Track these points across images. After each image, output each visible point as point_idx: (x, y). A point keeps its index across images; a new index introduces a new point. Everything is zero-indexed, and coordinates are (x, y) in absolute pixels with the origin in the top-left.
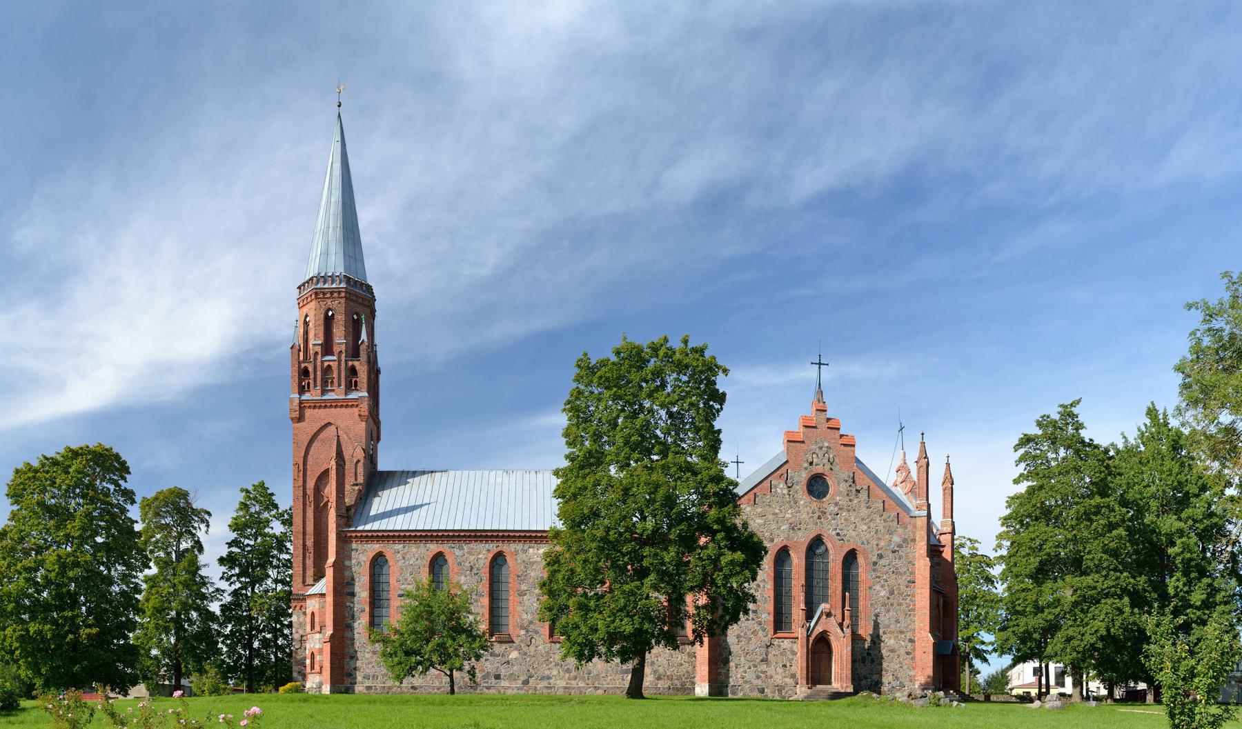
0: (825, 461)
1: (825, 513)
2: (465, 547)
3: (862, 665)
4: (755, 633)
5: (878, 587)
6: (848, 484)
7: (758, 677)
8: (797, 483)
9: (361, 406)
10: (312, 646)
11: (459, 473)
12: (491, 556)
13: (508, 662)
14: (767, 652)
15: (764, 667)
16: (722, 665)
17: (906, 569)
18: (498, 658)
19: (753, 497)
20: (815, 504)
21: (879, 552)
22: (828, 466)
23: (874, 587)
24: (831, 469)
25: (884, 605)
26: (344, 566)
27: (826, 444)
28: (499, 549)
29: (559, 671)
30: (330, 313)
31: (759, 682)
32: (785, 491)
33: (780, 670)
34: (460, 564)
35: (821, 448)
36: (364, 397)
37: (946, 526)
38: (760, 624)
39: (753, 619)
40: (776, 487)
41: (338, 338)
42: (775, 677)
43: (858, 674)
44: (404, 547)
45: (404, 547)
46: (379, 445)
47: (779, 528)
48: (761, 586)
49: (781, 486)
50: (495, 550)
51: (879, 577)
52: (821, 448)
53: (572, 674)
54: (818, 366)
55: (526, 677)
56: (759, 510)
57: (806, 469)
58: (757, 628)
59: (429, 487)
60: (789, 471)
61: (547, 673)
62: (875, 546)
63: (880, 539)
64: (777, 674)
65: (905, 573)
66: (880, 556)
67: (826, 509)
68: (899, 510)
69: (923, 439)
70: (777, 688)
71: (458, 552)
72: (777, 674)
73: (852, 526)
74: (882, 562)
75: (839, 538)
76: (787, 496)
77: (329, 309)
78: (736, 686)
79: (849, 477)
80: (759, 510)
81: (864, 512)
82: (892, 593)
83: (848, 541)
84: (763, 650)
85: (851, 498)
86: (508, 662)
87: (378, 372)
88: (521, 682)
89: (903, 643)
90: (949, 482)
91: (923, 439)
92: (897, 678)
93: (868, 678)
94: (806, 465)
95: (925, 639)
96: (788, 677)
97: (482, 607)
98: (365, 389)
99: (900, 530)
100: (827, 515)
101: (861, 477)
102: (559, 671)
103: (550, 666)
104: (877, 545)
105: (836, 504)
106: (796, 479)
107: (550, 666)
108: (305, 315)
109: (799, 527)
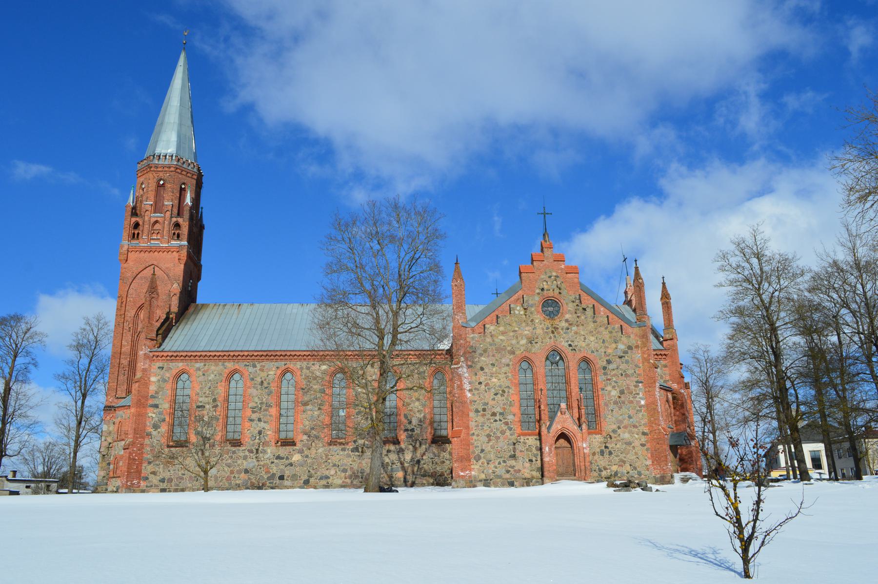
0: (555, 287)
1: (558, 328)
2: (258, 365)
3: (601, 457)
4: (503, 432)
5: (609, 388)
6: (575, 304)
7: (508, 472)
8: (532, 306)
9: (182, 252)
10: (116, 453)
11: (262, 305)
12: (279, 372)
13: (291, 465)
14: (515, 448)
15: (512, 462)
16: (475, 462)
17: (633, 371)
18: (282, 461)
19: (495, 318)
20: (548, 321)
21: (607, 358)
22: (557, 291)
23: (606, 388)
24: (560, 293)
25: (616, 403)
26: (150, 381)
27: (554, 274)
28: (286, 366)
29: (336, 472)
30: (162, 182)
31: (508, 476)
32: (522, 313)
33: (527, 465)
34: (252, 379)
35: (550, 277)
36: (184, 246)
37: (668, 333)
38: (506, 424)
39: (500, 420)
40: (514, 310)
41: (166, 201)
42: (523, 471)
43: (598, 466)
44: (205, 365)
45: (205, 365)
46: (199, 284)
47: (518, 343)
48: (506, 391)
49: (518, 308)
50: (284, 368)
51: (609, 380)
52: (550, 277)
53: (347, 474)
54: (546, 215)
55: (306, 477)
56: (502, 329)
57: (538, 294)
58: (505, 427)
59: (235, 317)
60: (524, 296)
61: (327, 473)
62: (603, 354)
63: (608, 347)
64: (524, 468)
65: (633, 375)
66: (609, 362)
67: (558, 325)
68: (622, 323)
69: (636, 265)
70: (525, 481)
71: (251, 369)
72: (524, 468)
73: (582, 338)
74: (611, 367)
75: (571, 348)
76: (524, 316)
77: (160, 180)
78: (488, 480)
79: (575, 298)
80: (502, 329)
81: (592, 325)
82: (622, 392)
83: (580, 350)
84: (511, 447)
85: (579, 315)
86: (291, 465)
87: (202, 227)
88: (302, 482)
89: (637, 436)
90: (665, 297)
91: (636, 265)
92: (635, 468)
93: (608, 469)
94: (538, 291)
95: (657, 431)
96: (534, 470)
97: (271, 416)
98: (186, 240)
99: (624, 339)
100: (560, 330)
101: (586, 298)
102: (336, 472)
103: (328, 467)
104: (605, 352)
105: (567, 321)
106: (531, 302)
107: (328, 467)
108: (141, 182)
109: (536, 341)
